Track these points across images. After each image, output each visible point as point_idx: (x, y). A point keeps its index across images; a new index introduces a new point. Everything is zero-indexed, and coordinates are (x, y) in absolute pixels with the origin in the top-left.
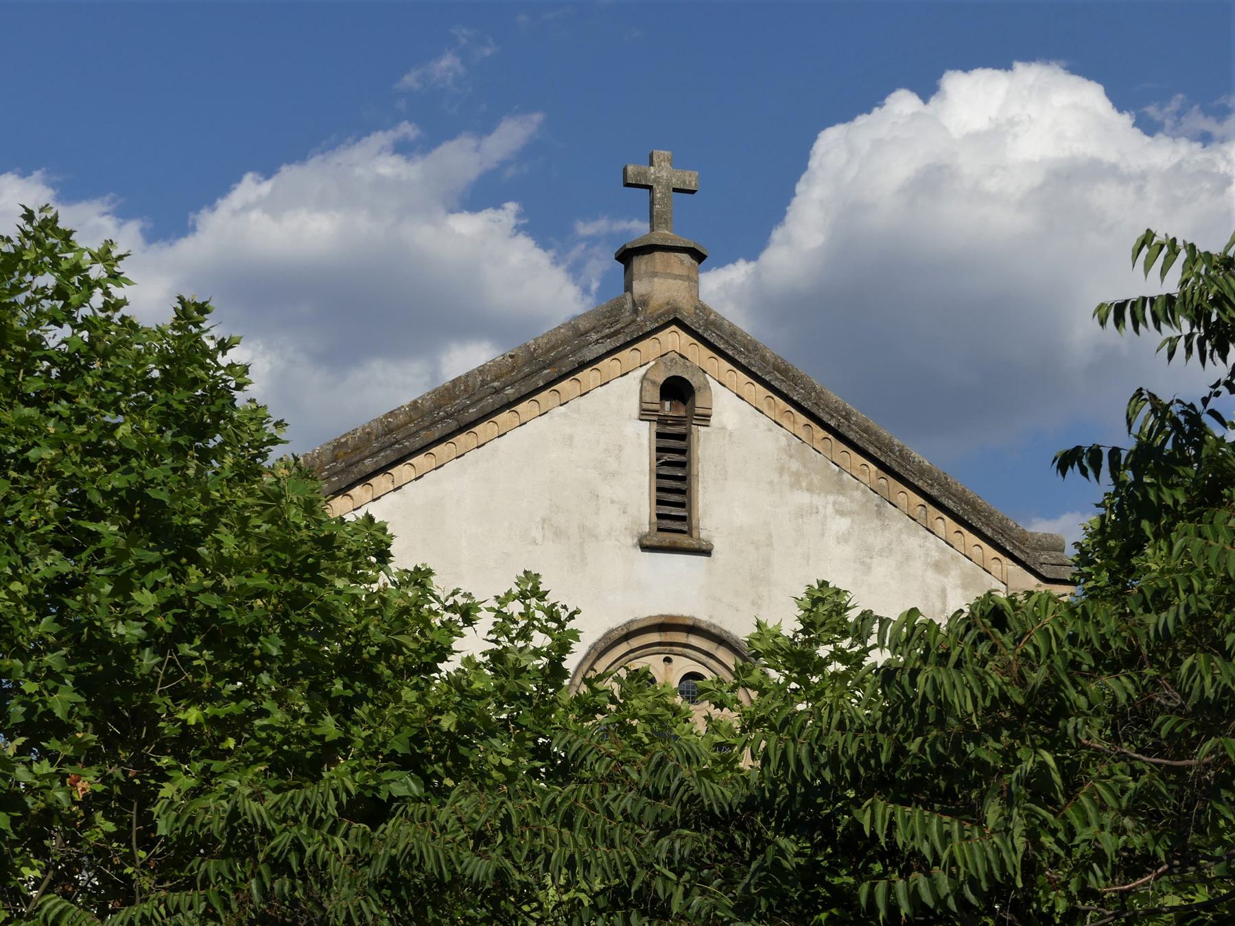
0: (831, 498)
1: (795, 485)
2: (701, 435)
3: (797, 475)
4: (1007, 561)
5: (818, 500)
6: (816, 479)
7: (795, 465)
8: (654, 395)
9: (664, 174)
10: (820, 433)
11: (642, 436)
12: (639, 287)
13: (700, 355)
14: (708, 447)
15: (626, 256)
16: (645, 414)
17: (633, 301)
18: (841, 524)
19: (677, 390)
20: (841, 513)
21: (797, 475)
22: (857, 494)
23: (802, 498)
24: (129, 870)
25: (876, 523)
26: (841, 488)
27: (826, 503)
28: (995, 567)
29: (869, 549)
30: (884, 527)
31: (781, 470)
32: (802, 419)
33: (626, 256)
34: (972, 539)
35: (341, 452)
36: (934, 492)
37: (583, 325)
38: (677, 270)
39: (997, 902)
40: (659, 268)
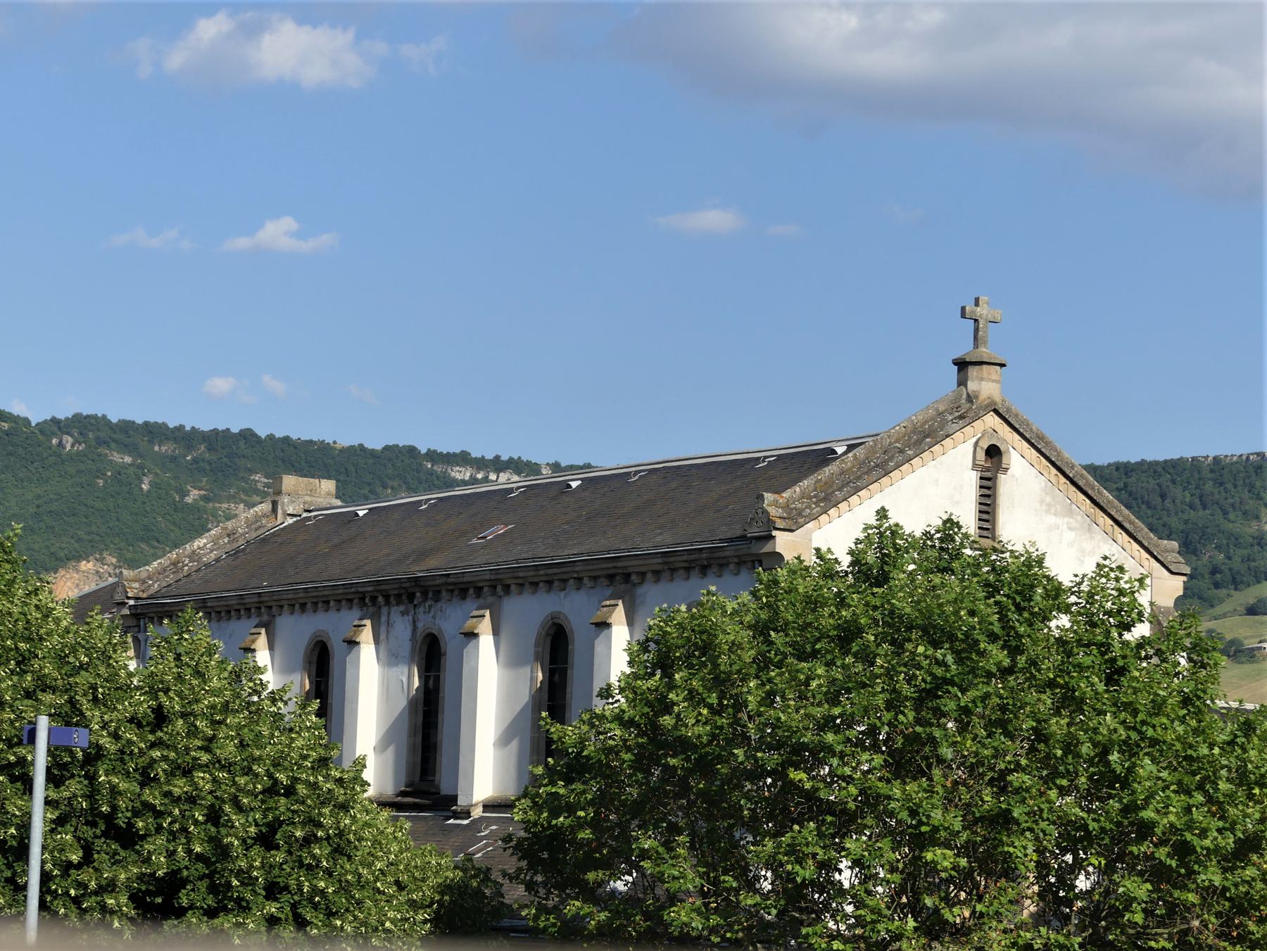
0: (1066, 520)
1: (1048, 511)
2: (1002, 478)
3: (1049, 505)
4: (1152, 560)
5: (1059, 521)
6: (1059, 507)
7: (1048, 499)
8: (981, 455)
9: (984, 312)
10: (1063, 480)
11: (972, 478)
12: (972, 385)
13: (1004, 430)
14: (1006, 485)
15: (962, 365)
16: (975, 466)
17: (968, 395)
18: (1070, 536)
19: (994, 452)
20: (1070, 529)
21: (1049, 505)
22: (1079, 518)
23: (1051, 519)
24: (195, 682)
25: (1088, 535)
26: (1070, 514)
27: (1063, 522)
28: (1146, 563)
29: (1083, 551)
30: (1092, 538)
31: (1042, 502)
32: (1054, 471)
33: (962, 365)
34: (1136, 546)
35: (818, 485)
36: (1120, 519)
37: (942, 408)
38: (994, 377)
39: (185, 494)
40: (985, 375)
